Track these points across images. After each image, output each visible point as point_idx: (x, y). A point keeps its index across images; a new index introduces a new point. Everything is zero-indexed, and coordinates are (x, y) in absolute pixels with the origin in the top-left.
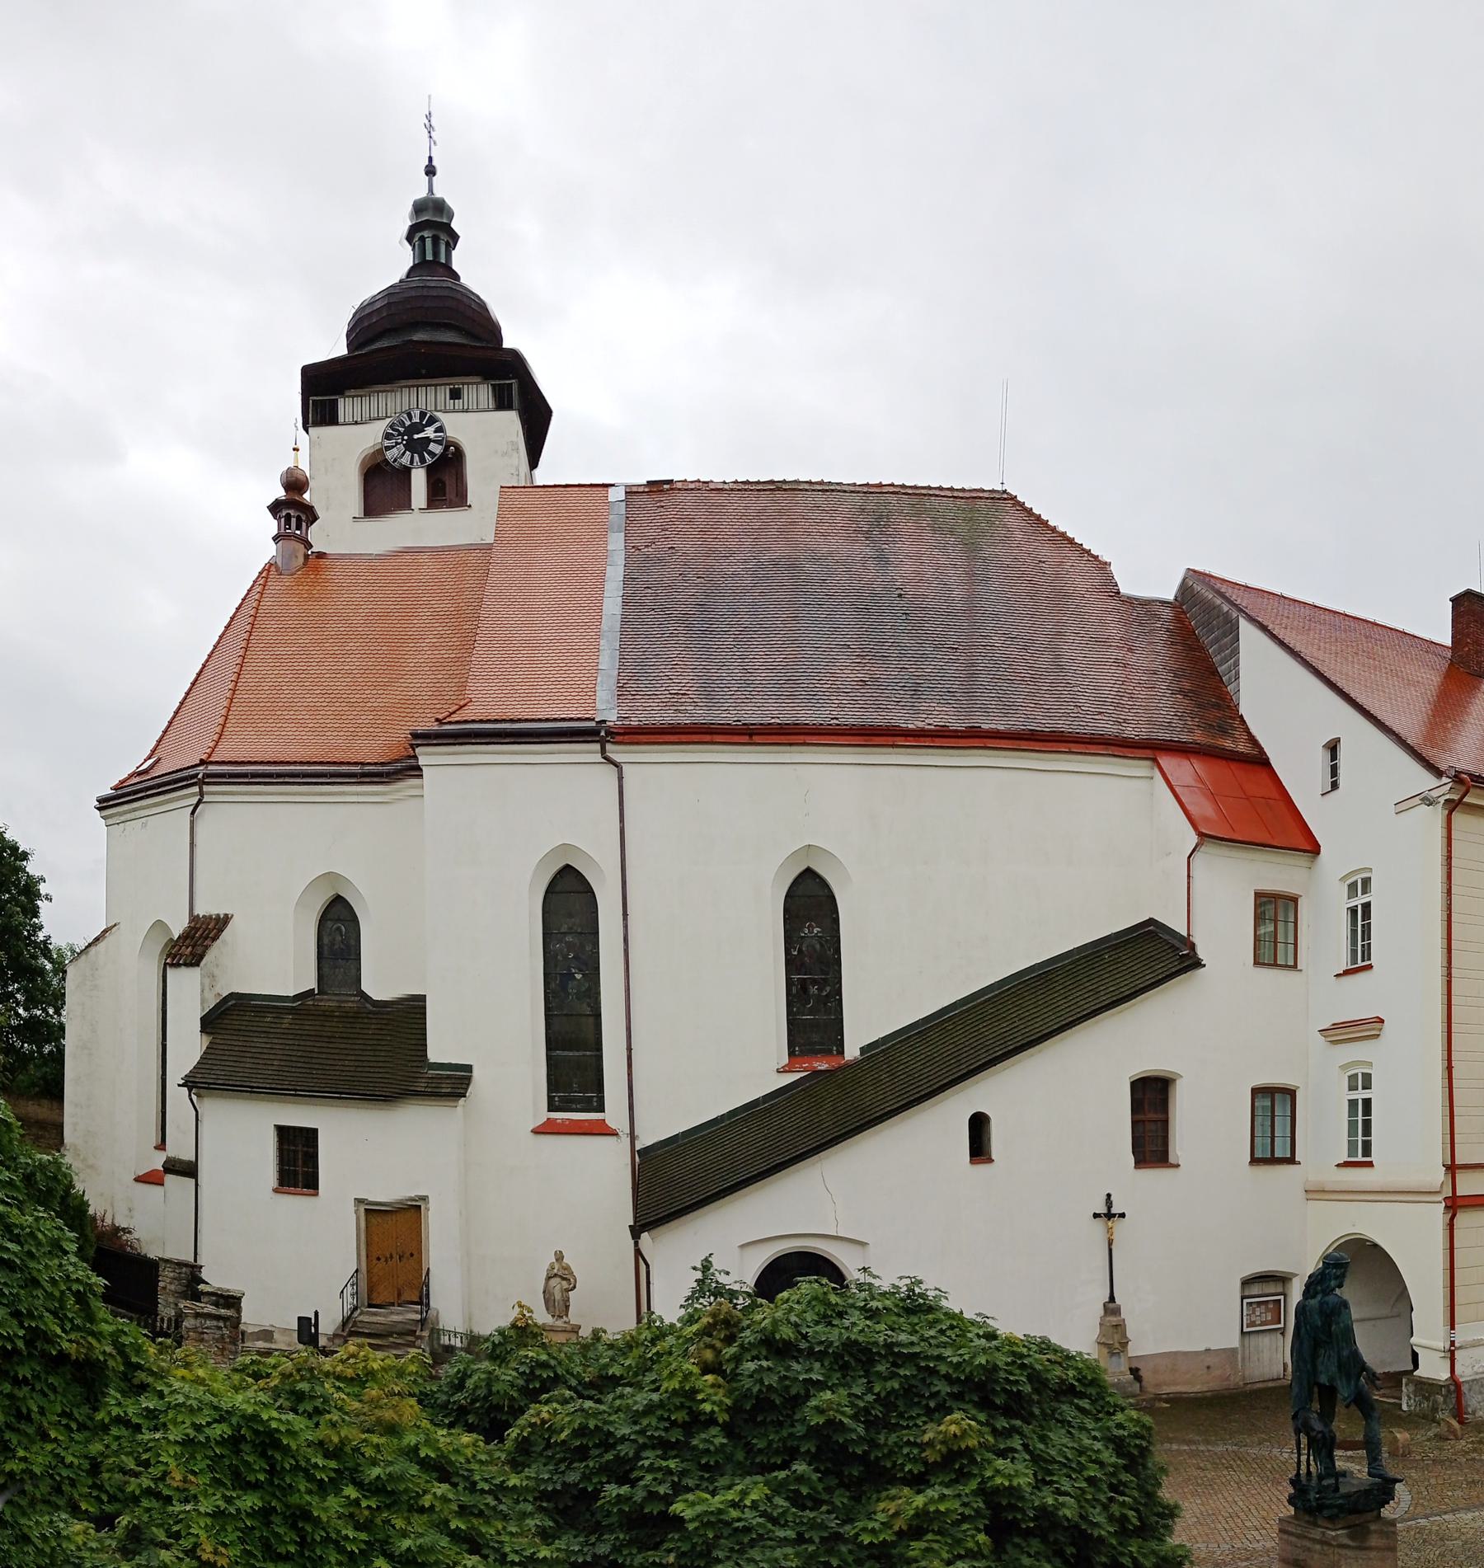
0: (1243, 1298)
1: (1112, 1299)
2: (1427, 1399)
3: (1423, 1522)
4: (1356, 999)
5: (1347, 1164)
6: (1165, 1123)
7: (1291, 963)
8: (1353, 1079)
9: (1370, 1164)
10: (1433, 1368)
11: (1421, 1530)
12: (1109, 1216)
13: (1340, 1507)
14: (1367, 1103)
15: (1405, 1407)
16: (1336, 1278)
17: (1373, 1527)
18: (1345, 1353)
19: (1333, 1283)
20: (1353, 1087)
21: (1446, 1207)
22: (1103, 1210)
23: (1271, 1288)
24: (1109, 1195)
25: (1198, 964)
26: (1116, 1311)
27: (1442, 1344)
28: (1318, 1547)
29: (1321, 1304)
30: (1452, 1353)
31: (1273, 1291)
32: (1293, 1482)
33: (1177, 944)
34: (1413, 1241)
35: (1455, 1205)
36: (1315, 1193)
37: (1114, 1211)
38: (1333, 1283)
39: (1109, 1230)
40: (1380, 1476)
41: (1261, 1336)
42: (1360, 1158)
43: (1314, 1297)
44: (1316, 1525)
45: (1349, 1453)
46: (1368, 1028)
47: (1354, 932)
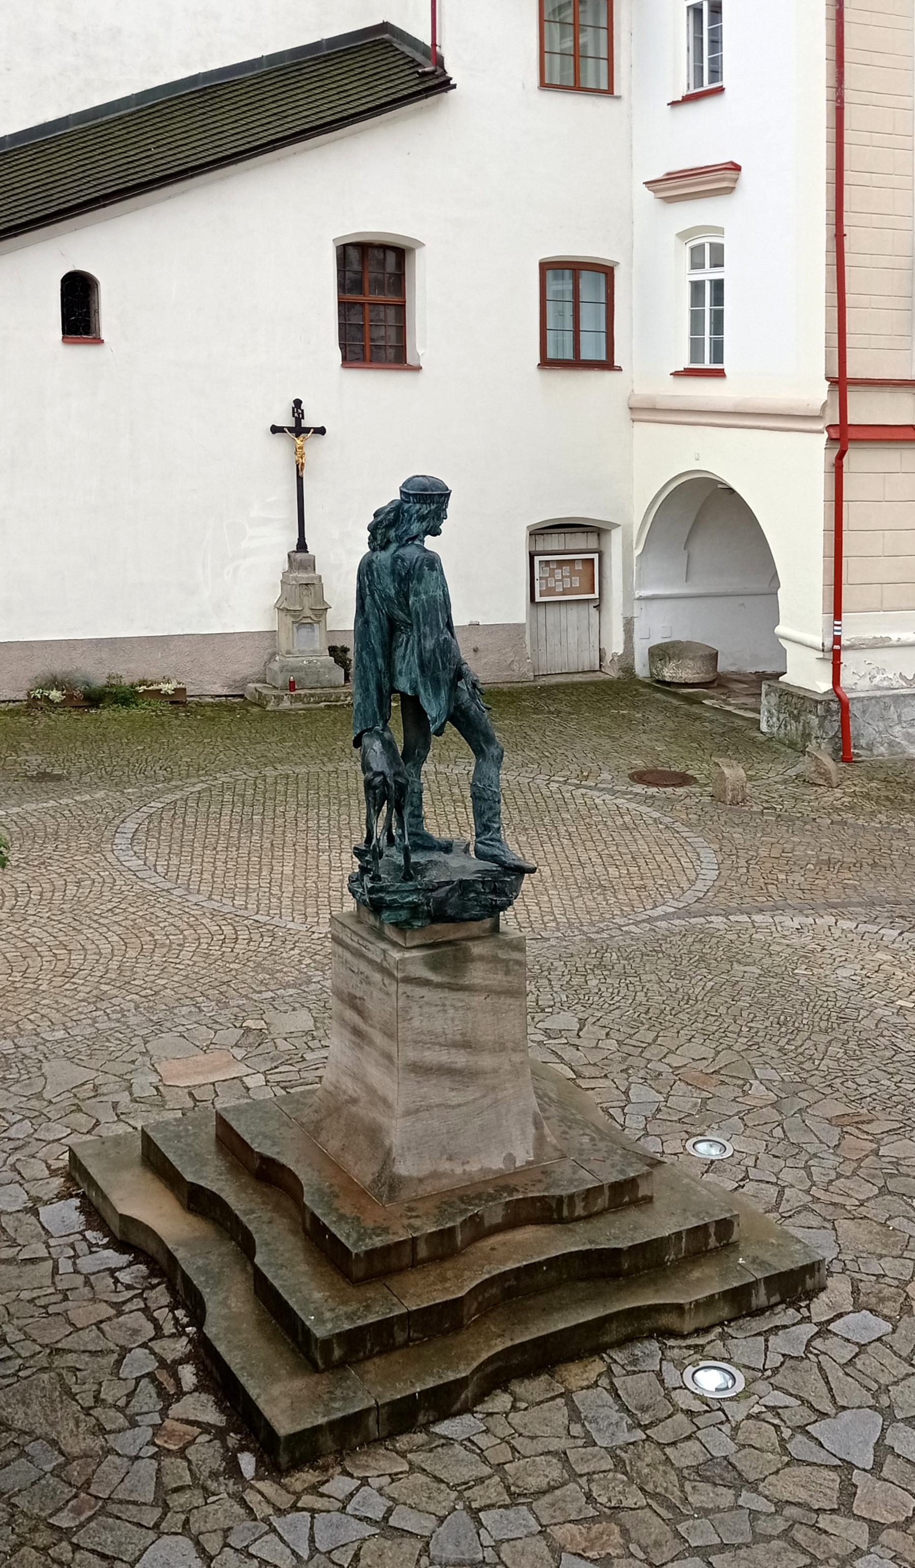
0: (532, 557)
1: (302, 546)
2: (796, 718)
3: (718, 921)
4: (699, 138)
5: (689, 373)
6: (401, 309)
7: (604, 86)
8: (696, 252)
9: (720, 374)
10: (808, 674)
11: (705, 935)
12: (298, 430)
13: (414, 908)
14: (718, 286)
15: (764, 727)
16: (422, 518)
17: (477, 949)
18: (429, 644)
19: (415, 527)
20: (697, 264)
21: (830, 439)
22: (287, 421)
23: (579, 541)
24: (298, 403)
25: (446, 85)
26: (310, 565)
27: (818, 637)
28: (377, 977)
29: (395, 559)
30: (837, 655)
31: (583, 546)
32: (359, 853)
33: (419, 58)
34: (782, 482)
35: (843, 437)
36: (644, 411)
37: (305, 424)
38: (415, 527)
39: (299, 452)
40: (493, 858)
41: (563, 608)
42: (707, 364)
43: (384, 548)
44: (380, 935)
45: (653, 790)
46: (717, 179)
47: (699, 41)
